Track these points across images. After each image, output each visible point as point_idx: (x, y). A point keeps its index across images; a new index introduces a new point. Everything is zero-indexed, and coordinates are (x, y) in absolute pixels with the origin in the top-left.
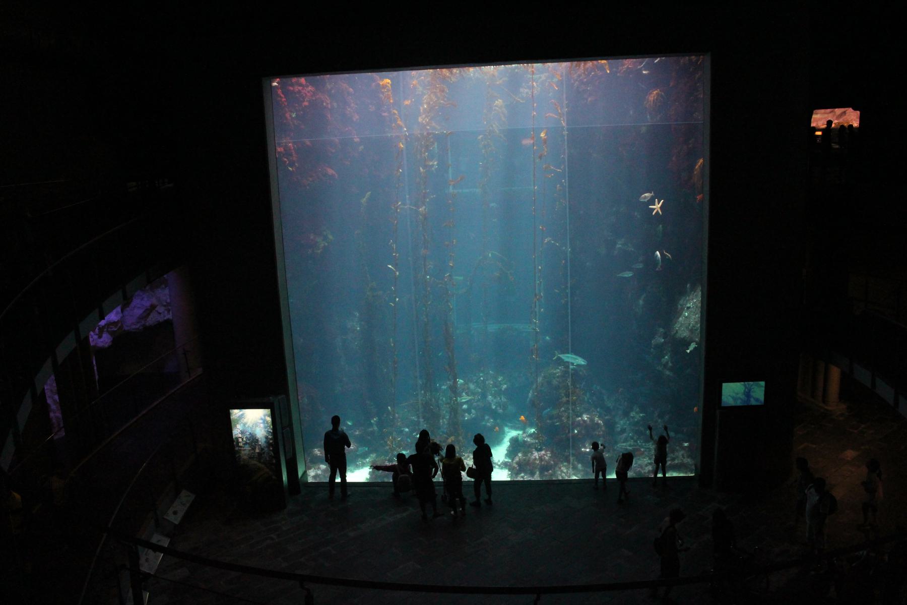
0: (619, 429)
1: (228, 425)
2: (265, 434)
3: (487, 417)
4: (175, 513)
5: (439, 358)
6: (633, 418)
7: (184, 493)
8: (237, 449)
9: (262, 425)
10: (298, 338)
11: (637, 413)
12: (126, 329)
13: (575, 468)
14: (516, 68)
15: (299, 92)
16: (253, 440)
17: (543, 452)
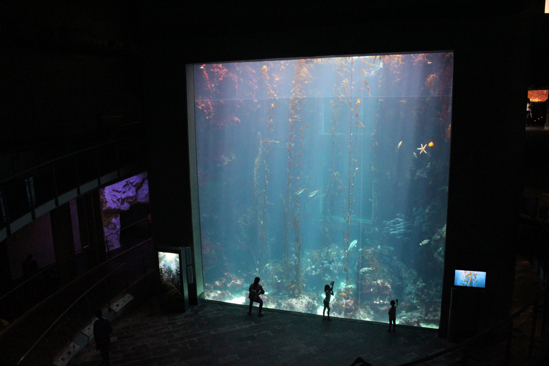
0: (407, 292)
1: (156, 260)
2: (176, 268)
3: (327, 275)
4: (117, 306)
5: (289, 237)
6: (418, 285)
9: (174, 263)
11: (420, 283)
12: (139, 201)
13: (369, 313)
14: (364, 59)
15: (218, 72)
16: (169, 271)
17: (349, 300)
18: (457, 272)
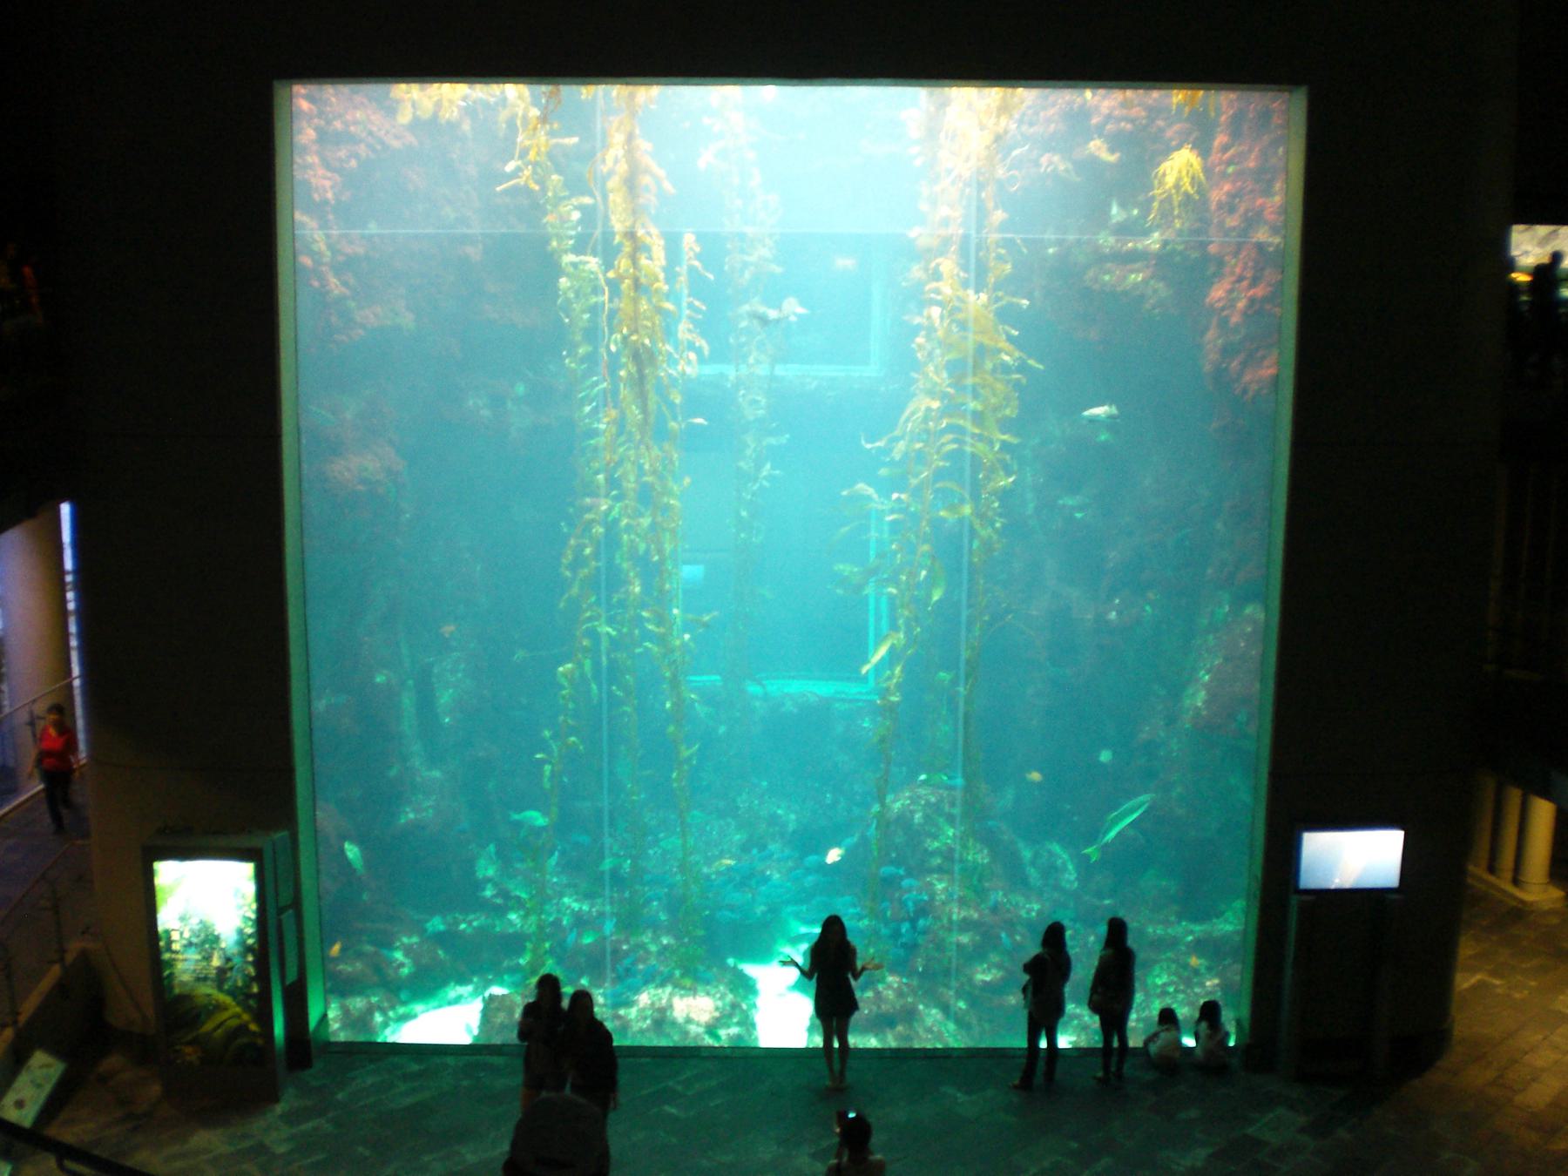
4: (20, 1104)
7: (39, 1058)
8: (166, 956)
10: (319, 701)
16: (207, 941)
18: (167, 873)
